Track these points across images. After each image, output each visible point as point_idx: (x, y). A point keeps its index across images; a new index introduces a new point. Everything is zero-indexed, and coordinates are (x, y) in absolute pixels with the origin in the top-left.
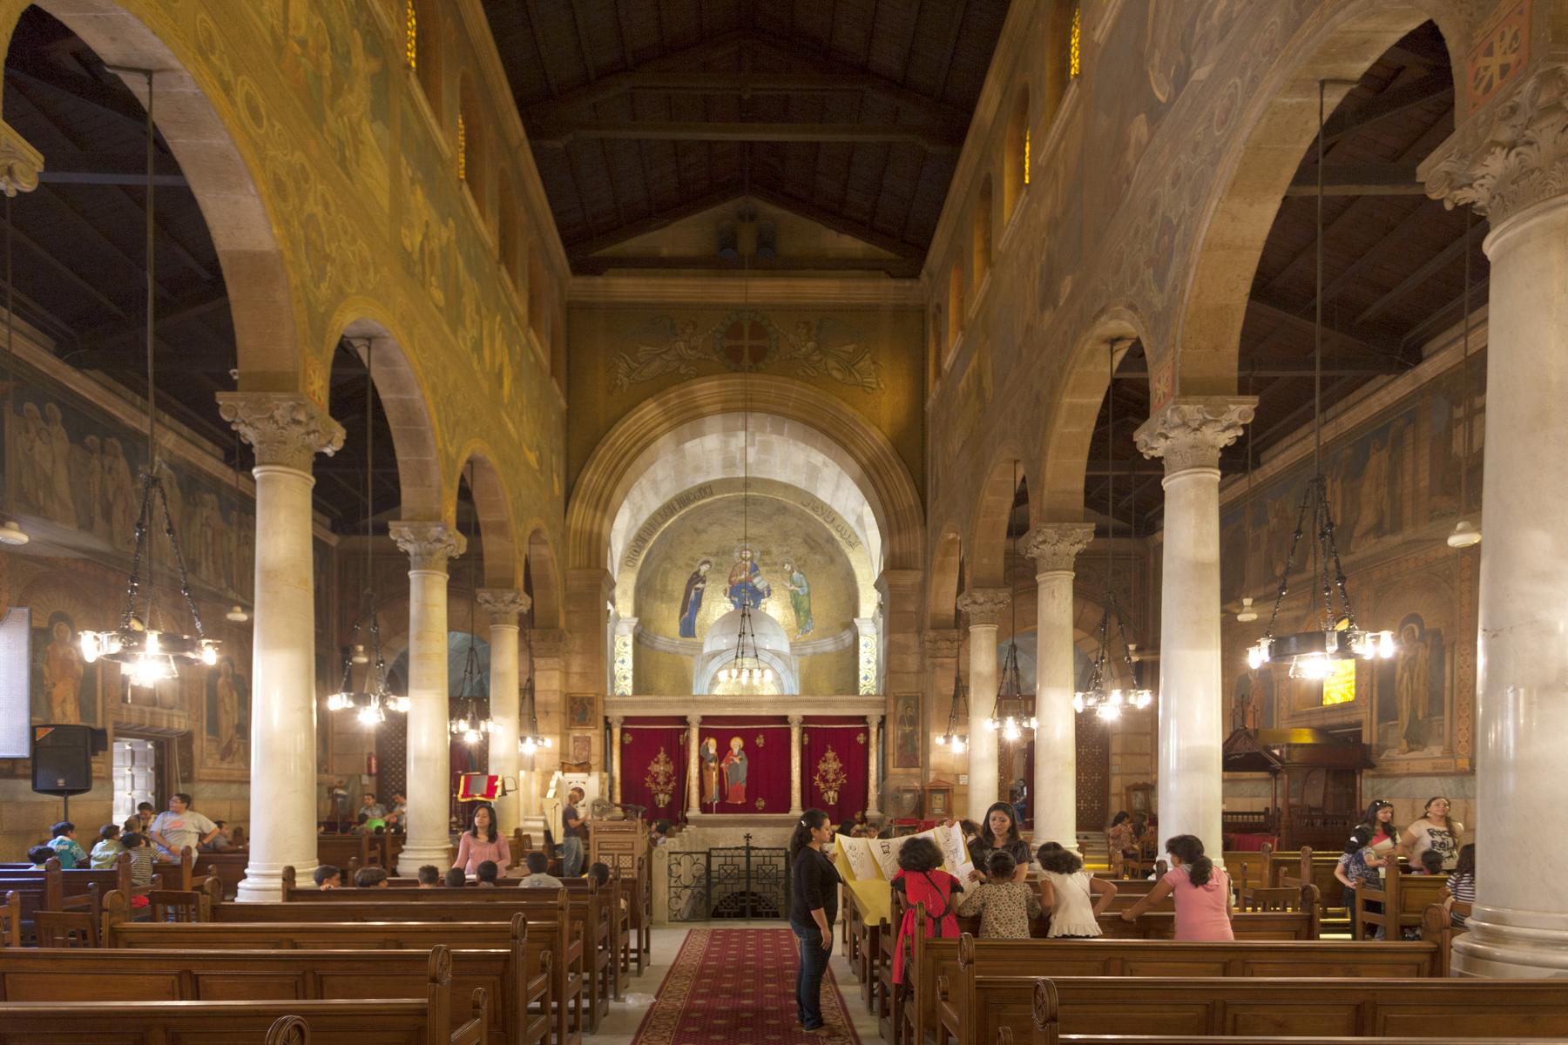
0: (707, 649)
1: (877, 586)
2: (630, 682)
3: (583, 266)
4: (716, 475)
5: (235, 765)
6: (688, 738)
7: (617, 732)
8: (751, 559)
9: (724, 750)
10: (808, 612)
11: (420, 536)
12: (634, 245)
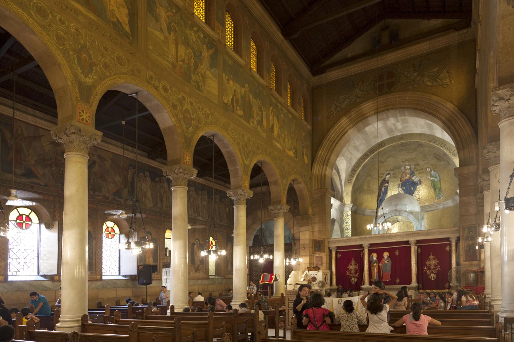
2: (350, 231)
3: (315, 73)
5: (200, 274)
6: (364, 254)
7: (334, 253)
8: (410, 169)
9: (380, 258)
11: (236, 194)
12: (338, 56)
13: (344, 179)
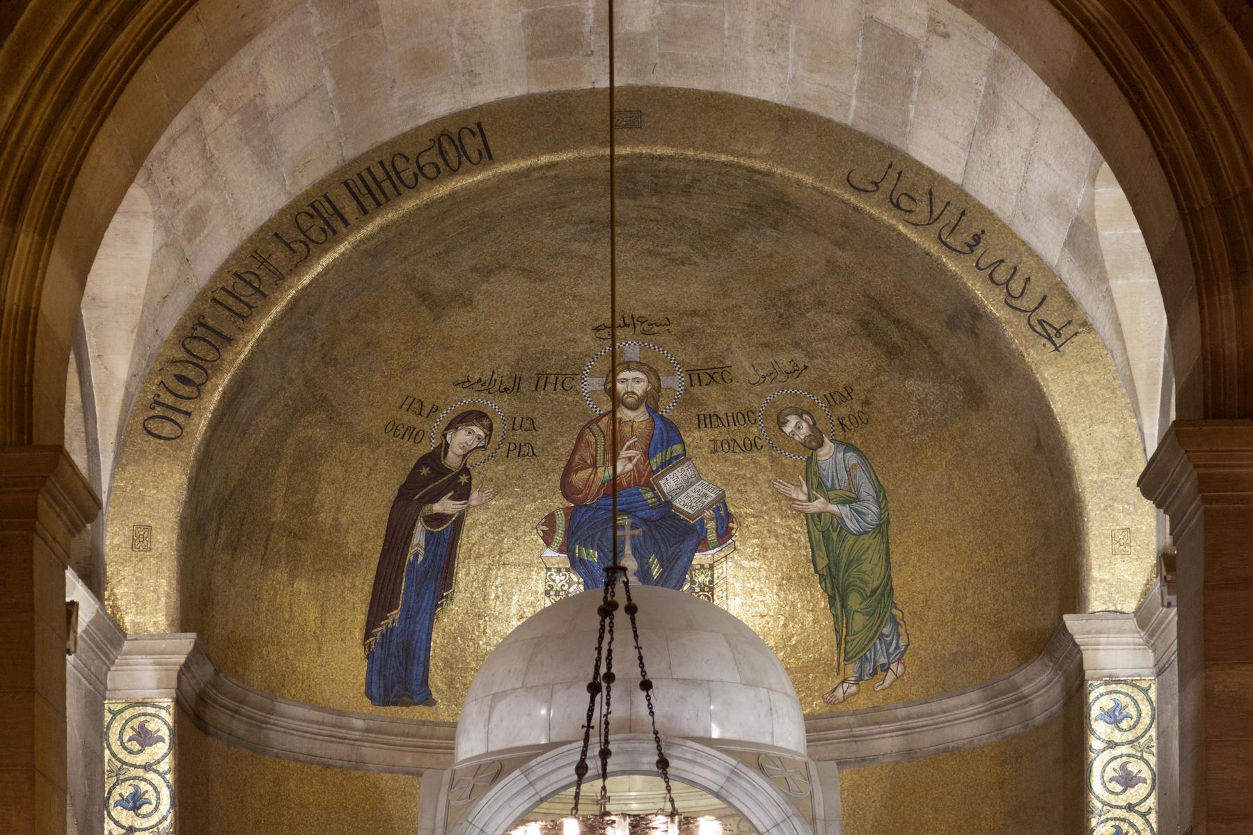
0: (470, 746)
1: (1153, 484)
4: (503, 82)
8: (650, 401)
10: (883, 595)
13: (118, 396)
